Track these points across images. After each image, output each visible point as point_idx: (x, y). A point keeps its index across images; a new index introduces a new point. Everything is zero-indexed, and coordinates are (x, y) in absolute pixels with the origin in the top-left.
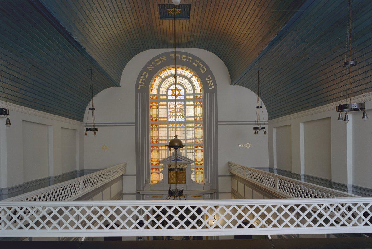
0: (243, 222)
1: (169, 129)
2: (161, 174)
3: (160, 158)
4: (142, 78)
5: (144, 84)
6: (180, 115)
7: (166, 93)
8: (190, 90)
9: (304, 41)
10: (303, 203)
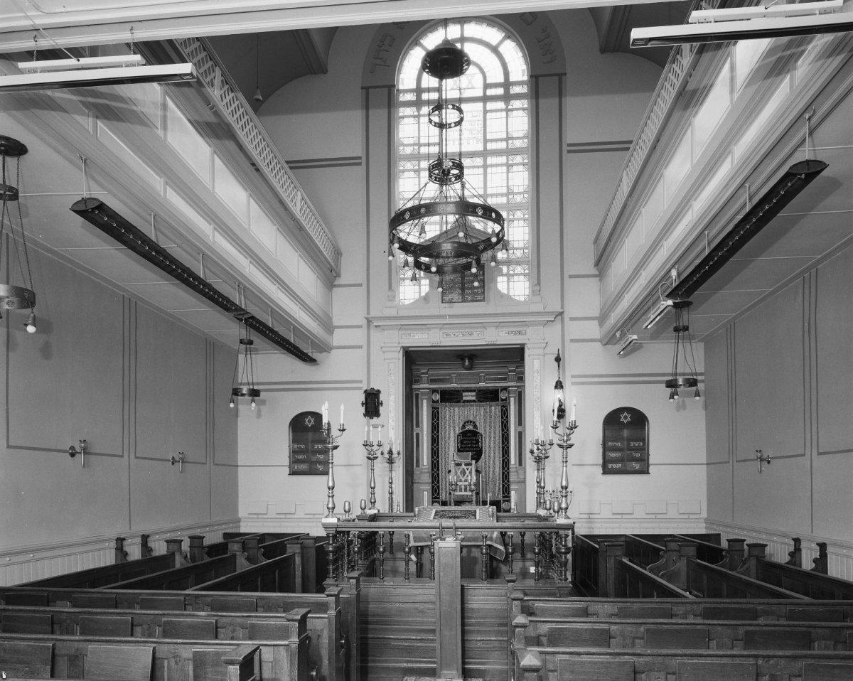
6: (471, 136)
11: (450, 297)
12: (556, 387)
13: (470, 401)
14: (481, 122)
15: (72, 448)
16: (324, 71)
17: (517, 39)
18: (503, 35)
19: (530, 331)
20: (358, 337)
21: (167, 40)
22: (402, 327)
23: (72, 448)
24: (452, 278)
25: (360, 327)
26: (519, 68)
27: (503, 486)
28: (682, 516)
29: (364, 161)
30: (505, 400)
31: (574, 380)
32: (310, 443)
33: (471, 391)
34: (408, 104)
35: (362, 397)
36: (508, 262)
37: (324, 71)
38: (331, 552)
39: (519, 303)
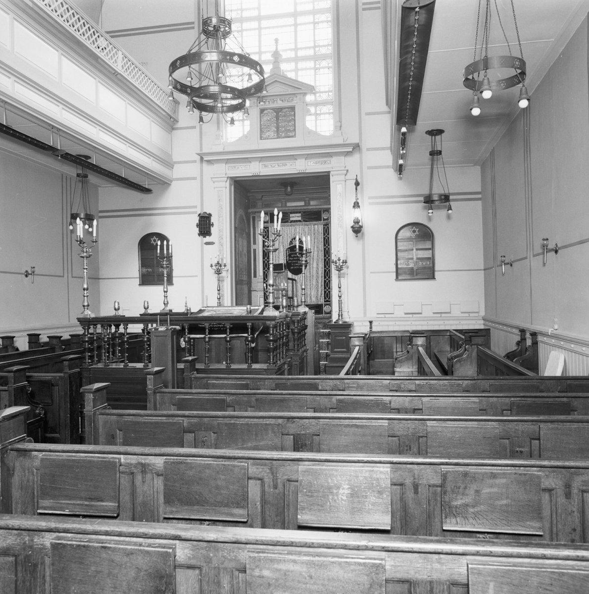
11: (268, 134)
12: (354, 207)
13: (297, 221)
15: (27, 271)
19: (334, 160)
20: (193, 170)
22: (228, 161)
23: (27, 271)
25: (195, 161)
27: (325, 292)
28: (463, 315)
30: (327, 219)
31: (371, 201)
32: (154, 261)
33: (297, 213)
35: (196, 220)
36: (316, 104)
38: (87, 341)
39: (325, 137)
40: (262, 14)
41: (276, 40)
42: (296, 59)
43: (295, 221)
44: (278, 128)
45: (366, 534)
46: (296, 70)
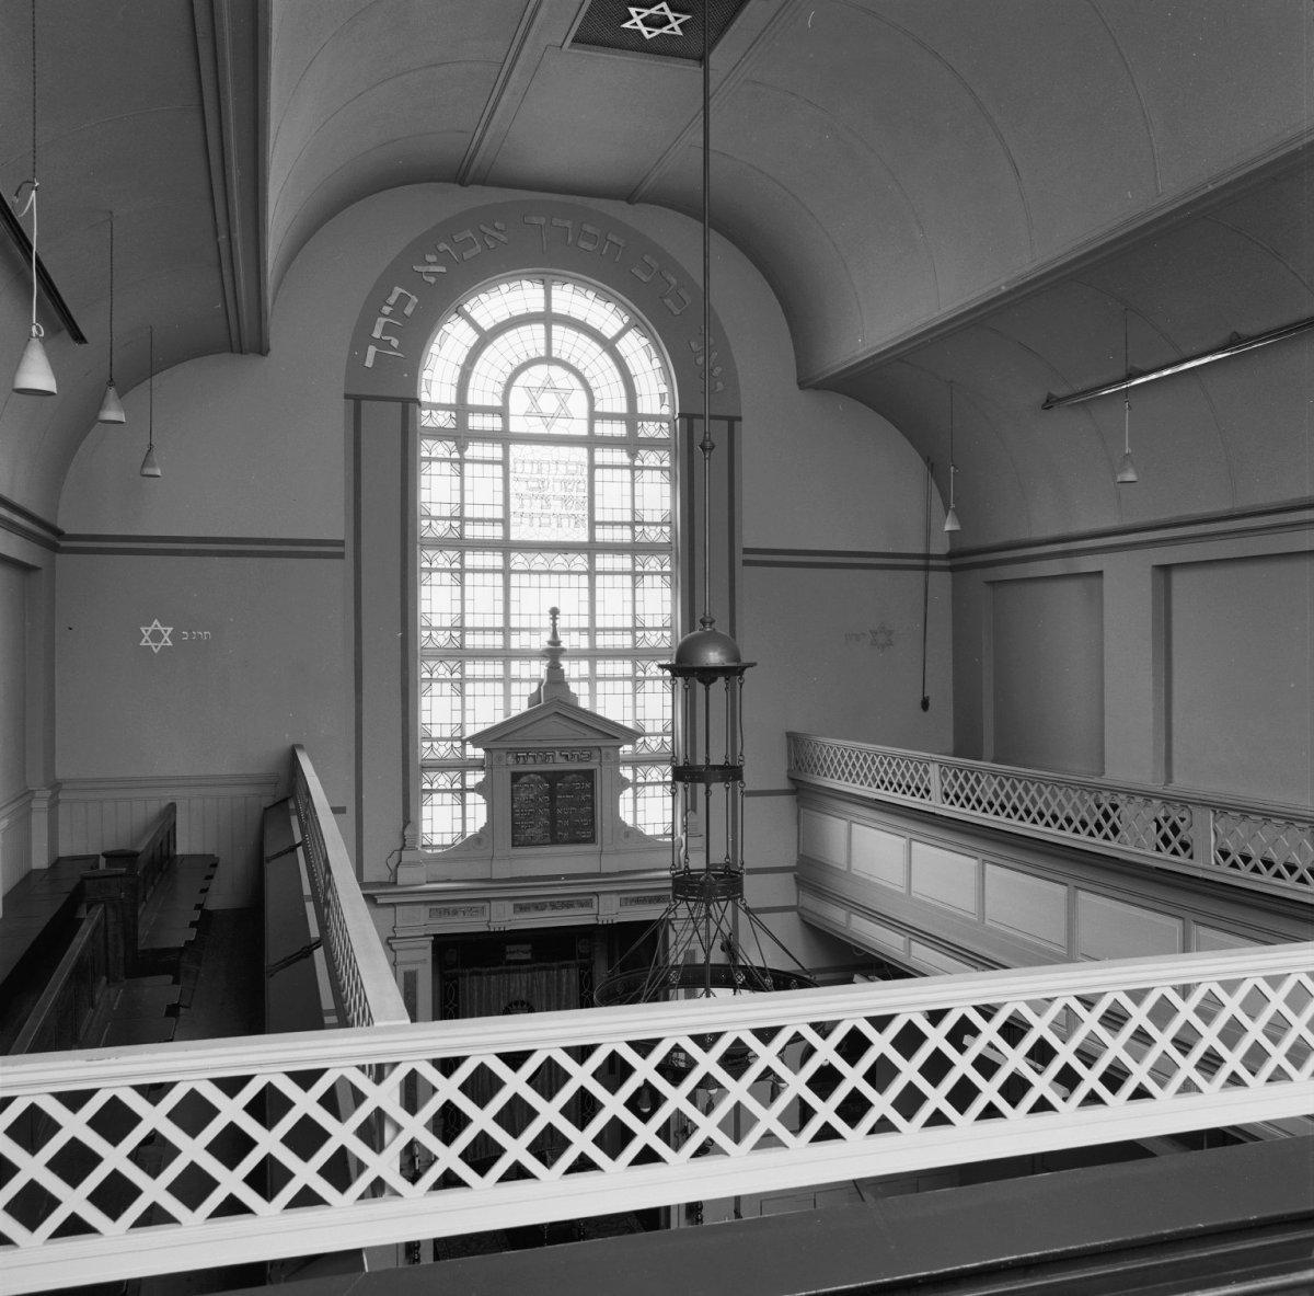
0: (342, 1150)
1: (514, 579)
2: (470, 797)
3: (469, 717)
4: (385, 316)
5: (395, 343)
6: (564, 511)
7: (498, 403)
8: (612, 399)
9: (111, 383)
10: (611, 1034)
14: (584, 486)
16: (262, 349)
17: (652, 334)
18: (626, 319)
21: (358, 1159)
24: (531, 796)
26: (655, 392)
29: (349, 549)
34: (440, 434)
36: (636, 762)
37: (262, 349)
40: (513, 537)
41: (554, 612)
42: (593, 655)
43: (517, 962)
44: (553, 818)
45: (1099, 556)
46: (592, 679)
